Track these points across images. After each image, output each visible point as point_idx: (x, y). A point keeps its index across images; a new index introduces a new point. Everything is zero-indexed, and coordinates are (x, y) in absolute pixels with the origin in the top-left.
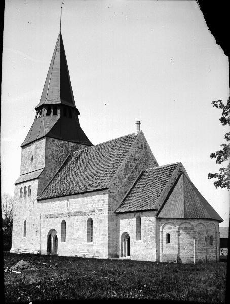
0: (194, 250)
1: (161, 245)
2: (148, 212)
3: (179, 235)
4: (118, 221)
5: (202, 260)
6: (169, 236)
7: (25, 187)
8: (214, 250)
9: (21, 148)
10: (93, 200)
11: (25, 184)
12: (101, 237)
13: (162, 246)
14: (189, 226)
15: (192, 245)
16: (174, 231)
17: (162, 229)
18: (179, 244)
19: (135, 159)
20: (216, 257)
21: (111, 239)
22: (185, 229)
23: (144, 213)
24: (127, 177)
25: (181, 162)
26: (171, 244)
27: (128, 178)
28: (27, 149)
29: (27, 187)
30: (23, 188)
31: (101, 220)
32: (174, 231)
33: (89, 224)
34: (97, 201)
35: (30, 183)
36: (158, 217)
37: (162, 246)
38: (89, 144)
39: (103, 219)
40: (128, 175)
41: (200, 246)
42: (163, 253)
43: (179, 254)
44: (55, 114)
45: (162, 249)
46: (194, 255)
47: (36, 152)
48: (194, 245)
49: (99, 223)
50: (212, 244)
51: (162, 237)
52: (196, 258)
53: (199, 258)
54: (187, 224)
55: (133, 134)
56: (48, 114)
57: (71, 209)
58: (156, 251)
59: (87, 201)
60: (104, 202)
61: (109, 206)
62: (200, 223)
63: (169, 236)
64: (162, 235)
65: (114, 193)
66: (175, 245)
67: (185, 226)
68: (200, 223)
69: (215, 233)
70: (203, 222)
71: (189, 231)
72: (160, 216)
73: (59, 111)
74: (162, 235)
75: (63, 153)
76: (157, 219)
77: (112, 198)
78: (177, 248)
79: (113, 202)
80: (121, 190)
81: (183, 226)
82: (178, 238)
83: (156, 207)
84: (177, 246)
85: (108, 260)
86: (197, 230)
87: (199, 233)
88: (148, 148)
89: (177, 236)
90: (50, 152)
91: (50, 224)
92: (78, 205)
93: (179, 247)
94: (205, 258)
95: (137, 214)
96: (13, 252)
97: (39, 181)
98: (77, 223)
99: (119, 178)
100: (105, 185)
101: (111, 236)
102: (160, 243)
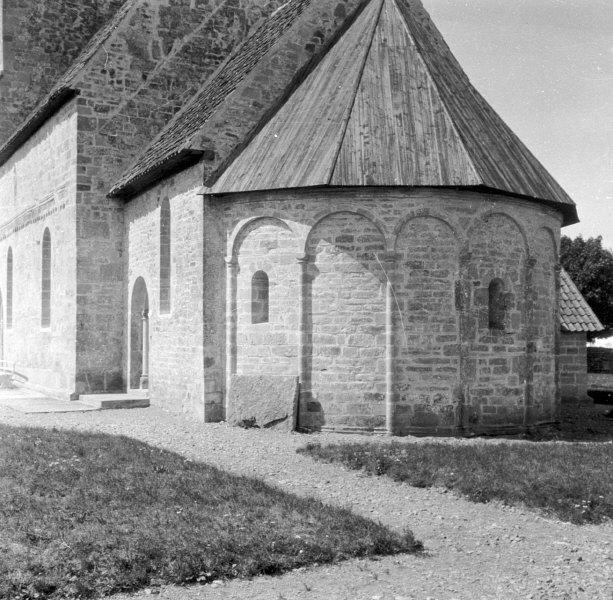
0: (388, 358)
1: (228, 333)
3: (307, 279)
4: (124, 231)
5: (436, 410)
6: (261, 281)
8: (508, 356)
13: (234, 338)
14: (360, 229)
15: (377, 330)
17: (235, 253)
18: (307, 326)
20: (529, 388)
21: (92, 311)
22: (344, 242)
24: (178, 45)
27: (186, 49)
32: (285, 261)
33: (259, 284)
36: (217, 189)
37: (234, 338)
38: (563, 226)
40: (186, 39)
41: (426, 335)
42: (240, 372)
43: (307, 377)
45: (234, 351)
46: (388, 382)
48: (388, 333)
51: (234, 292)
52: (395, 398)
53: (414, 397)
54: (352, 219)
58: (208, 362)
61: (81, 169)
62: (425, 215)
63: (261, 281)
64: (234, 282)
65: (105, 110)
66: (288, 333)
67: (338, 232)
68: (425, 215)
69: (520, 268)
70: (437, 205)
71: (375, 256)
72: (231, 180)
74: (234, 282)
75: (78, 23)
76: (207, 197)
77: (93, 135)
78: (300, 345)
79: (102, 152)
80: (149, 101)
81: (332, 230)
82: (306, 293)
83: (205, 140)
84: (299, 334)
86: (405, 252)
87: (415, 266)
89: (299, 286)
90: (24, 19)
93: (308, 338)
94: (450, 399)
99: (136, 50)
101: (92, 295)
102: (229, 324)
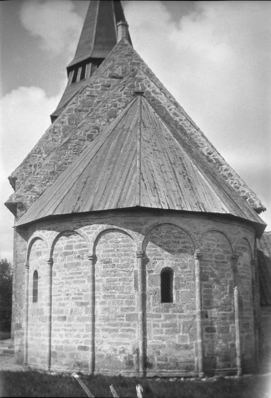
68: (113, 230)
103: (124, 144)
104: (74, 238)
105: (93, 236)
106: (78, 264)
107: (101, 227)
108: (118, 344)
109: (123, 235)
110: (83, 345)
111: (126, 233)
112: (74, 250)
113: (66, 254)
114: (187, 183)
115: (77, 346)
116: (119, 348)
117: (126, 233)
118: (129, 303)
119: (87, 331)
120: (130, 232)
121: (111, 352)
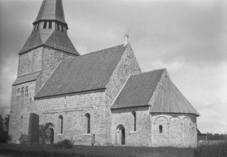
2: (141, 108)
7: (23, 88)
9: (19, 55)
10: (91, 98)
11: (23, 85)
12: (99, 129)
16: (165, 123)
19: (125, 65)
23: (138, 108)
24: (119, 80)
25: (165, 69)
26: (163, 134)
28: (24, 56)
29: (25, 87)
30: (21, 88)
31: (99, 115)
34: (94, 99)
35: (27, 84)
39: (100, 114)
44: (50, 27)
47: (33, 59)
49: (96, 118)
50: (22, 117)
55: (123, 45)
56: (45, 27)
57: (68, 105)
59: (85, 99)
60: (102, 100)
68: (186, 118)
73: (53, 24)
85: (39, 125)
87: (184, 125)
88: (134, 57)
91: (47, 118)
92: (75, 102)
95: (133, 110)
96: (43, 22)
97: (36, 82)
98: (74, 118)
100: (102, 85)
103: (74, 102)
104: (176, 118)
105: (183, 118)
106: (178, 125)
107: (185, 116)
108: (187, 144)
109: (188, 120)
110: (179, 144)
111: (188, 118)
112: (177, 121)
113: (174, 122)
114: (88, 105)
115: (178, 144)
116: (187, 145)
117: (188, 118)
118: (189, 134)
119: (76, 112)
120: (189, 118)
121: (185, 145)
